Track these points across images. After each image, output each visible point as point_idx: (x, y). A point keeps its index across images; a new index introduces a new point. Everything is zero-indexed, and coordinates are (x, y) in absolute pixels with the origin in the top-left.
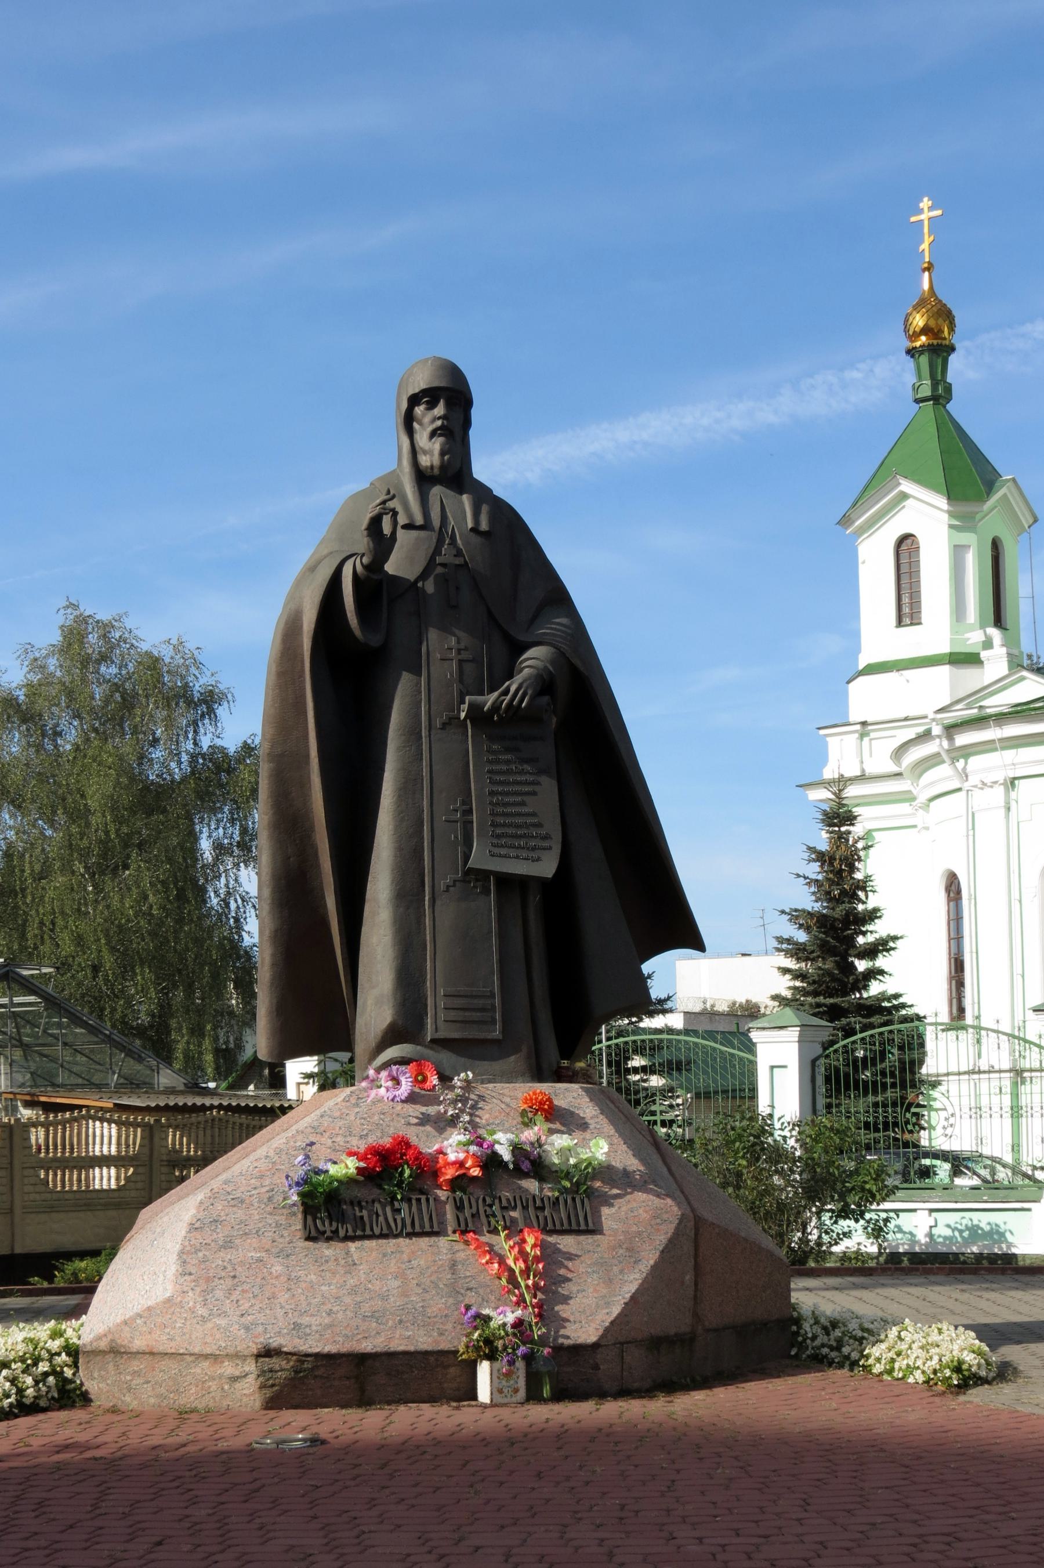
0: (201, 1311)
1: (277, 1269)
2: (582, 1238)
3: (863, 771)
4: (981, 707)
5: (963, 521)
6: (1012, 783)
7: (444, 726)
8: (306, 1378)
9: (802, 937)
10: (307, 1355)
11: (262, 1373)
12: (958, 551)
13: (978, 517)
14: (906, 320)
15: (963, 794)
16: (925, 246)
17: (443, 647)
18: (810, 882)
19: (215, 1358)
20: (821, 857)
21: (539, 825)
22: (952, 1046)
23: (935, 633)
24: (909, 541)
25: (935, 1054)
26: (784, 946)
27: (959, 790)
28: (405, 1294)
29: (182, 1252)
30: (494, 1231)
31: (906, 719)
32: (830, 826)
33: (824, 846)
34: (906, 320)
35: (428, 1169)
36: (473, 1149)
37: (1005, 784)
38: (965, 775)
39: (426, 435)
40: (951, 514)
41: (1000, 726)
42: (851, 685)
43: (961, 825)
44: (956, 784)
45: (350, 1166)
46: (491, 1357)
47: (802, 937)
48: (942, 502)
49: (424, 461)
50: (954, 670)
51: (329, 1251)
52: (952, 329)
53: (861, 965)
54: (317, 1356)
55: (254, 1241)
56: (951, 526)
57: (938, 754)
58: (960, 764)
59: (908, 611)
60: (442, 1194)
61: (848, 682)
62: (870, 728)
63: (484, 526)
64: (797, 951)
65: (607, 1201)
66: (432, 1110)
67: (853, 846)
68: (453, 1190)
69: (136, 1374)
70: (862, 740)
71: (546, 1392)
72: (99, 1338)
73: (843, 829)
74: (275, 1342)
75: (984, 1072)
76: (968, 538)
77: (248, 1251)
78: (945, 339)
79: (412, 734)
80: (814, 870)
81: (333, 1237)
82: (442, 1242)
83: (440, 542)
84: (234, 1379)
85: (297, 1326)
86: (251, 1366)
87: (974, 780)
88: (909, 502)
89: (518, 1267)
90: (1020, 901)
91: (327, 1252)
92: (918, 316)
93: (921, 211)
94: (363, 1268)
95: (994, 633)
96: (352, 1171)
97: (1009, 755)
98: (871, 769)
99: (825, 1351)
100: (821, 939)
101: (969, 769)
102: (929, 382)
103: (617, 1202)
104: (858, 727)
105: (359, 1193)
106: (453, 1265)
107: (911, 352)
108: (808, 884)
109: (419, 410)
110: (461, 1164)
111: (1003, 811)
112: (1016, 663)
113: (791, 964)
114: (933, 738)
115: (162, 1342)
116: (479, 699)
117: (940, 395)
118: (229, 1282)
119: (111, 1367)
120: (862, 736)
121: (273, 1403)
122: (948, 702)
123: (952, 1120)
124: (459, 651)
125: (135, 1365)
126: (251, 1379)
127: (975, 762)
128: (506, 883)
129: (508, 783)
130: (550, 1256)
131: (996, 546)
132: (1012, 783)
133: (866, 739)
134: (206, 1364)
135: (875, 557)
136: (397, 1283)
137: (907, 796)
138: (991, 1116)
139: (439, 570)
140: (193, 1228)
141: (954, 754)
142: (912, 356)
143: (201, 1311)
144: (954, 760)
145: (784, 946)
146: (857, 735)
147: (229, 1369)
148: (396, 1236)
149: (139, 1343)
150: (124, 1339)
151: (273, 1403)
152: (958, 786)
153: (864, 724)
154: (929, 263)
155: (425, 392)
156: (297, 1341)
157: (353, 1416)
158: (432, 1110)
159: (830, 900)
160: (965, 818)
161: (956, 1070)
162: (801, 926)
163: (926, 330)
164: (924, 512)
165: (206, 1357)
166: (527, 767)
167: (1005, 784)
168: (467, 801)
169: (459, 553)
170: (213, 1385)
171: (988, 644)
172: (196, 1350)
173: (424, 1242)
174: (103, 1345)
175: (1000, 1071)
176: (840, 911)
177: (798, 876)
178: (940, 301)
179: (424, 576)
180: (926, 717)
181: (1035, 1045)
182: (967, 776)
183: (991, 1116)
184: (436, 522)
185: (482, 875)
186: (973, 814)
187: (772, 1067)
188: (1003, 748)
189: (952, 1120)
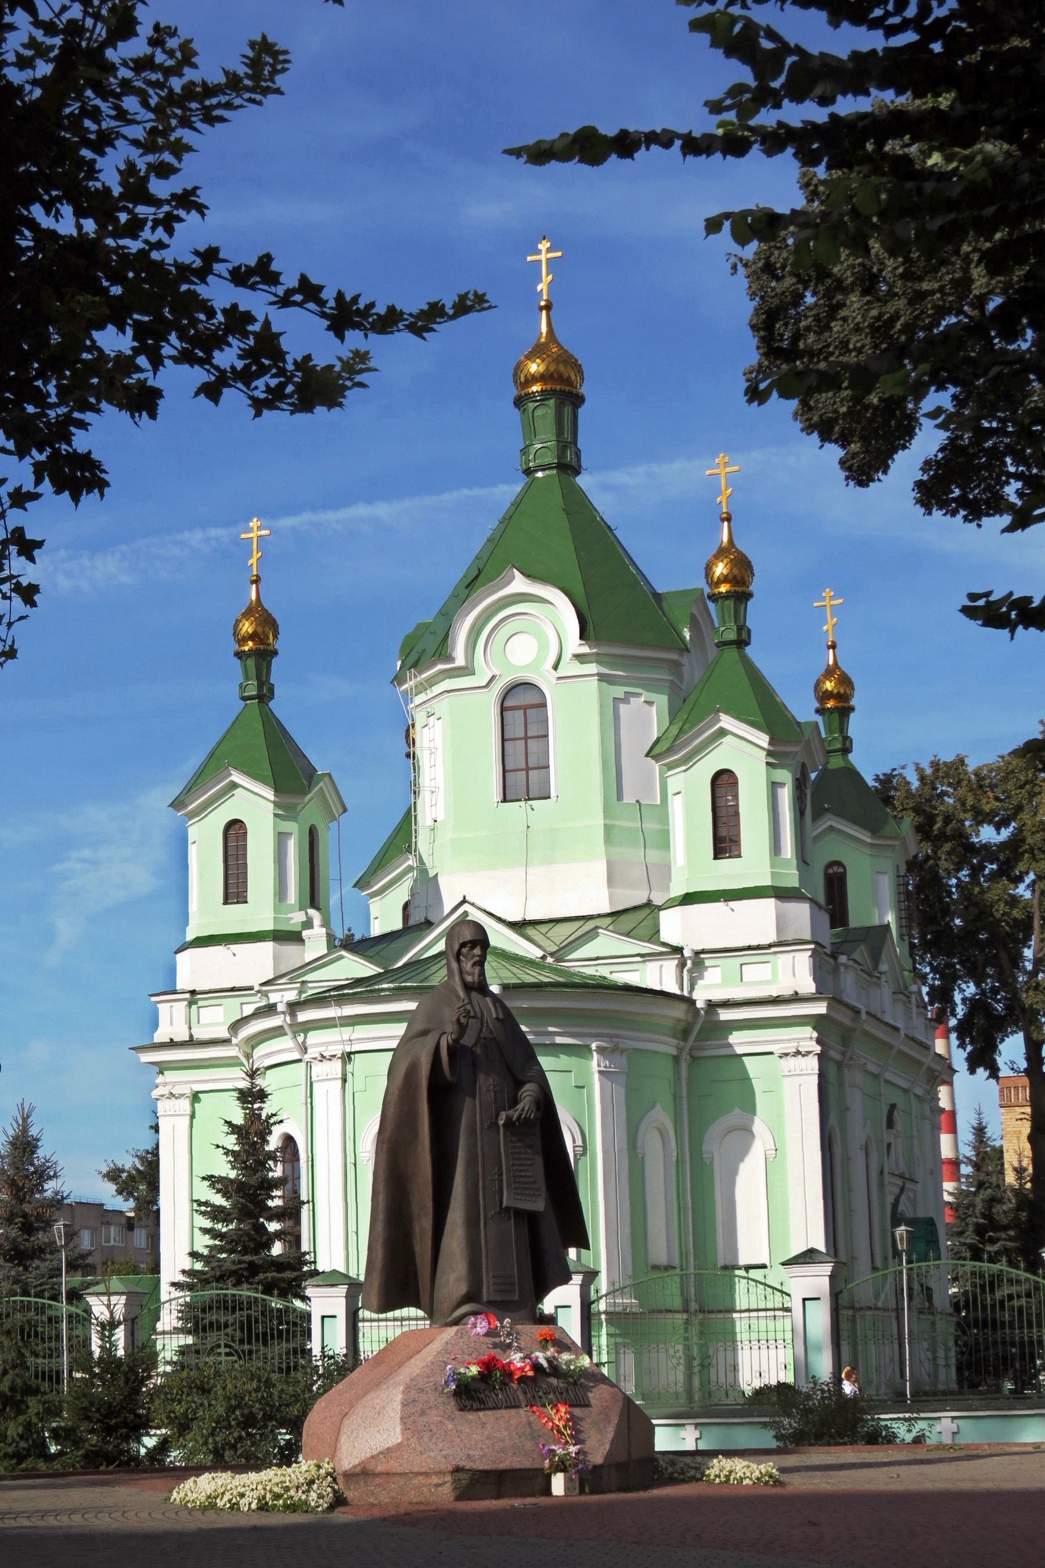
0: (419, 1448)
1: (450, 1426)
2: (583, 1409)
3: (191, 1036)
4: (303, 982)
5: (285, 810)
6: (347, 1057)
7: (489, 1127)
8: (476, 1482)
9: (219, 1200)
10: (477, 1471)
11: (455, 1481)
12: (281, 838)
13: (299, 807)
14: (236, 625)
15: (303, 1065)
16: (253, 561)
17: (486, 1083)
18: (227, 1152)
19: (426, 1474)
20: (234, 1128)
21: (535, 1183)
23: (259, 911)
24: (237, 826)
26: (203, 1208)
27: (299, 1061)
28: (511, 1439)
29: (401, 1419)
30: (544, 1406)
31: (233, 989)
32: (244, 1103)
33: (239, 1119)
34: (236, 625)
35: (508, 1373)
36: (528, 1361)
37: (342, 1058)
38: (304, 1049)
39: (469, 964)
40: (276, 804)
41: (340, 1006)
42: (179, 956)
43: (301, 1092)
44: (296, 1056)
45: (474, 1370)
46: (564, 1470)
47: (219, 1200)
48: (270, 794)
49: (469, 979)
50: (277, 946)
51: (471, 1416)
52: (275, 637)
54: (482, 1471)
55: (434, 1412)
56: (276, 815)
57: (281, 1027)
58: (300, 1039)
59: (235, 891)
60: (514, 1386)
61: (176, 953)
62: (198, 996)
63: (501, 1016)
64: (216, 1213)
65: (589, 1389)
66: (497, 1340)
67: (266, 1121)
68: (519, 1384)
69: (379, 1485)
70: (190, 1007)
71: (587, 1490)
72: (355, 1467)
73: (256, 1106)
74: (461, 1464)
75: (368, 1321)
76: (291, 827)
77: (434, 1417)
78: (269, 644)
79: (472, 1131)
80: (231, 1142)
81: (471, 1409)
82: (521, 1411)
83: (482, 1025)
84: (437, 1486)
85: (469, 1456)
86: (448, 1478)
87: (313, 1052)
88: (238, 791)
89: (561, 1424)
90: (355, 1165)
91: (470, 1417)
92: (247, 624)
93: (251, 530)
94: (489, 1426)
95: (312, 912)
96: (476, 1373)
97: (346, 1032)
98: (200, 1034)
99: (676, 1475)
100: (242, 1204)
101: (309, 1042)
102: (255, 683)
103: (594, 1390)
104: (188, 996)
105: (477, 1385)
106: (530, 1423)
107: (239, 655)
108: (225, 1154)
109: (464, 950)
110: (522, 1369)
111: (339, 1082)
112: (332, 943)
113: (208, 1224)
114: (278, 1013)
115: (394, 1466)
116: (511, 1112)
117: (265, 694)
118: (429, 1433)
119: (362, 1483)
120: (191, 1003)
121: (458, 1498)
122: (271, 976)
124: (494, 1086)
125: (378, 1481)
126: (448, 1485)
127: (314, 1038)
128: (518, 1213)
129: (520, 1159)
130: (573, 1418)
131: (313, 833)
132: (347, 1057)
133: (194, 1007)
134: (421, 1478)
135: (205, 839)
136: (506, 1433)
137: (237, 1061)
139: (483, 1041)
140: (405, 1404)
141: (295, 1029)
142: (240, 658)
143: (419, 1448)
144: (295, 1035)
145: (203, 1208)
146: (186, 1003)
147: (435, 1480)
148: (499, 1409)
149: (380, 1468)
150: (371, 1466)
151: (458, 1498)
152: (299, 1057)
153: (193, 992)
154: (257, 575)
155: (470, 942)
156: (471, 1464)
157: (494, 1502)
158: (497, 1340)
159: (246, 1168)
160: (303, 1087)
162: (219, 1191)
163: (252, 637)
164: (253, 802)
165: (421, 1474)
166: (529, 1151)
167: (342, 1058)
168: (500, 1169)
169: (491, 1032)
170: (425, 1489)
171: (308, 924)
172: (416, 1470)
173: (513, 1411)
174: (358, 1470)
176: (254, 1180)
177: (218, 1146)
178: (266, 611)
179: (475, 1045)
180: (251, 988)
182: (306, 1049)
184: (479, 1015)
185: (508, 1209)
186: (311, 1083)
187: (323, 1317)
188: (342, 1026)
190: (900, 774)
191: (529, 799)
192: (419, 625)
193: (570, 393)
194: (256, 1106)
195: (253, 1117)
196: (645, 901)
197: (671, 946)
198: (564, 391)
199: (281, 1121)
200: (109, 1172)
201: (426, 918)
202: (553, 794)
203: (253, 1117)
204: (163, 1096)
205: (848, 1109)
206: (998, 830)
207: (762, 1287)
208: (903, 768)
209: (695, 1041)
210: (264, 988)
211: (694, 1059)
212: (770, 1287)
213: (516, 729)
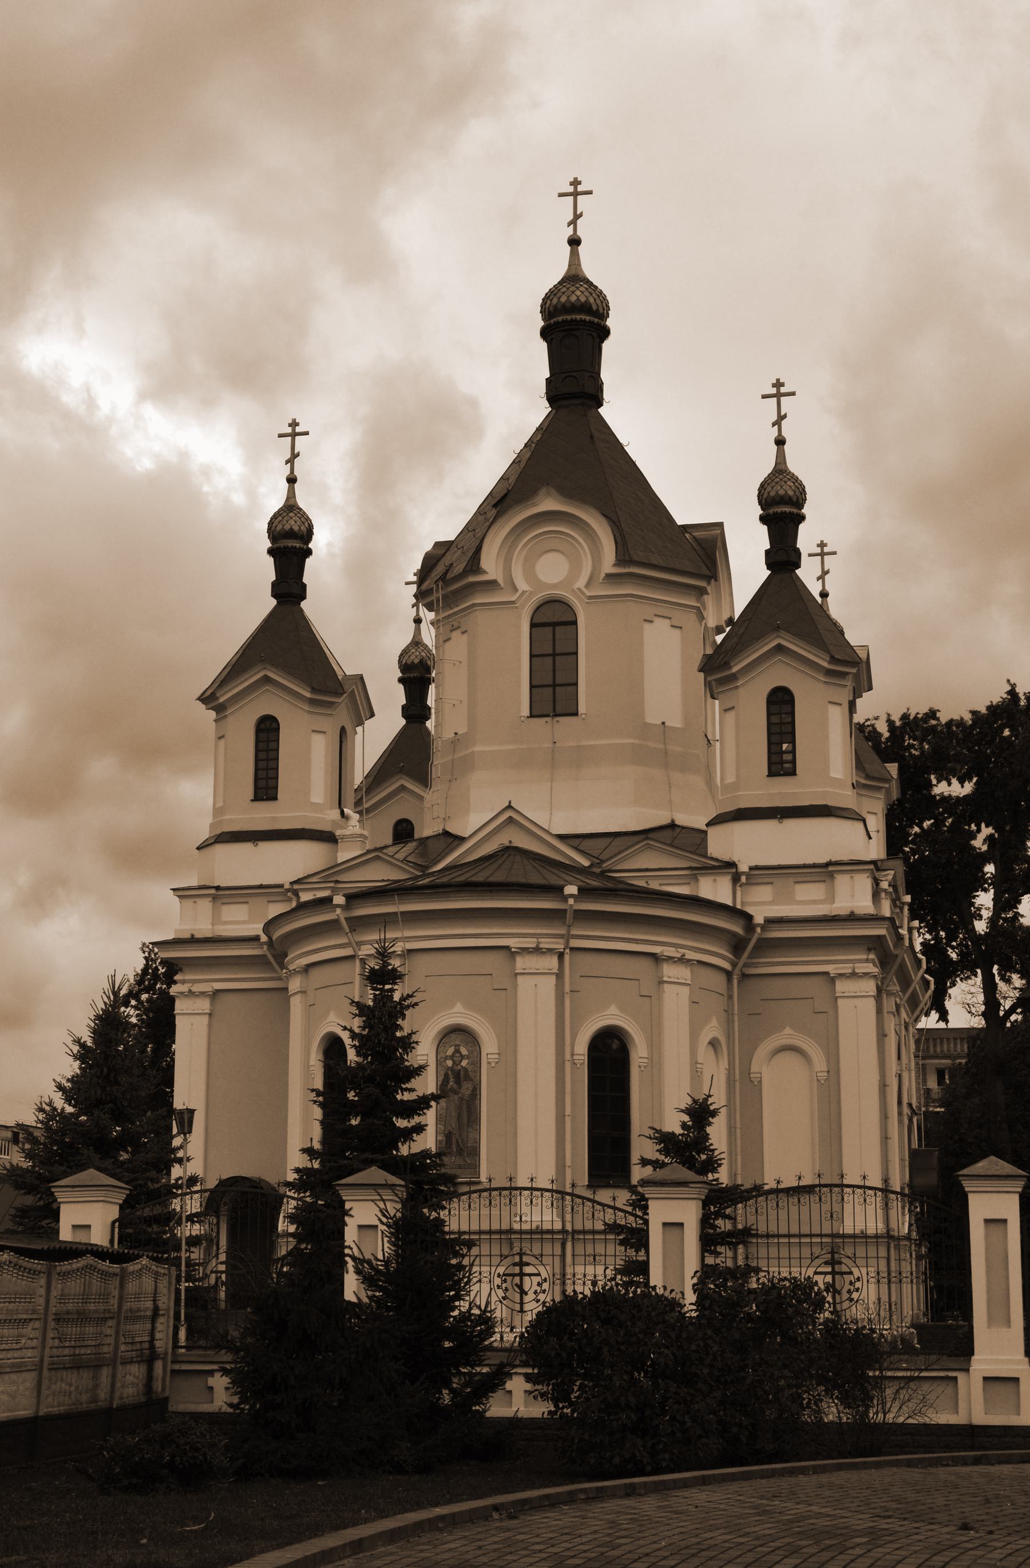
20: (362, 1009)
22: (794, 1210)
25: (840, 1216)
31: (261, 887)
53: (401, 1123)
67: (400, 1003)
73: (387, 987)
75: (762, 1236)
123: (858, 1285)
138: (585, 1276)
161: (829, 1232)
175: (779, 1236)
180: (281, 886)
181: (609, 1207)
183: (585, 1276)
189: (858, 1285)
190: (873, 725)
191: (556, 715)
192: (438, 545)
193: (599, 325)
194: (387, 987)
195: (383, 999)
196: (668, 821)
197: (721, 861)
198: (593, 322)
199: (416, 1004)
200: (73, 1077)
201: (444, 830)
202: (582, 709)
203: (383, 999)
204: (182, 993)
205: (886, 1036)
206: (962, 783)
207: (590, 1204)
208: (876, 718)
209: (749, 957)
210: (296, 887)
211: (744, 976)
212: (599, 1204)
213: (262, 783)
